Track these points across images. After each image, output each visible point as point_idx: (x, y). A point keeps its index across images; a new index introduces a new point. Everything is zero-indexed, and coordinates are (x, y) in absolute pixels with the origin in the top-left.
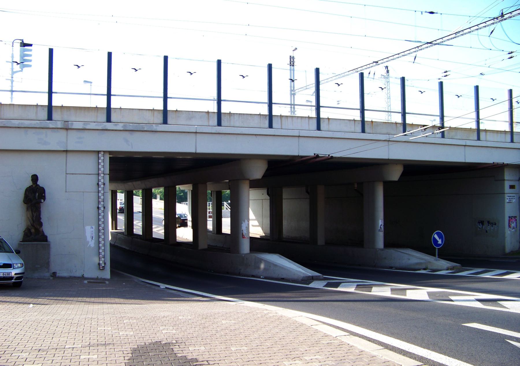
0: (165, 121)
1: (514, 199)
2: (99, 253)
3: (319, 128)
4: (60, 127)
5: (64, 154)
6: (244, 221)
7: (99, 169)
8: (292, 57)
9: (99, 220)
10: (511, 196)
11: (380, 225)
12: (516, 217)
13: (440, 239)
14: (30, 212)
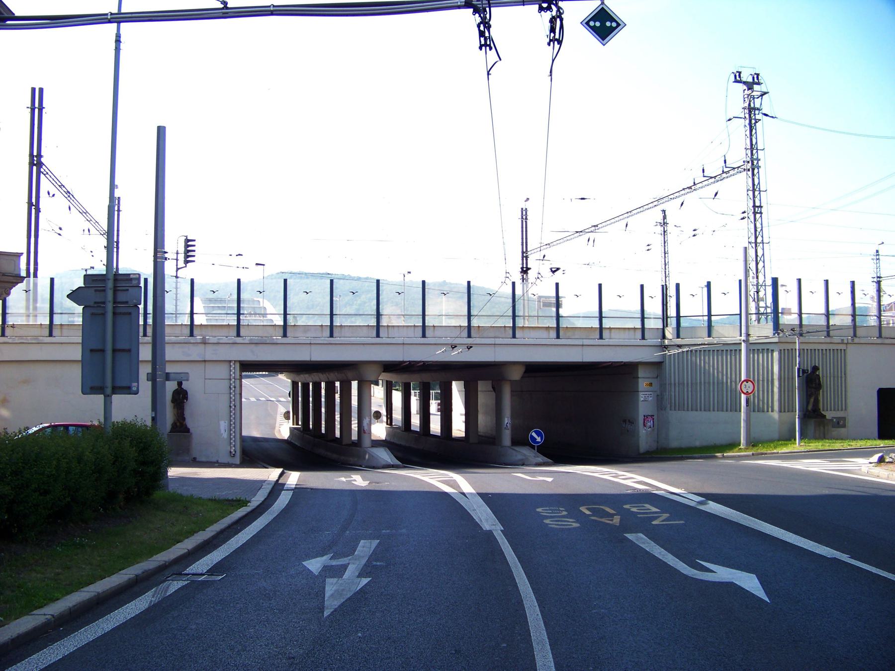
0: (285, 335)
1: (651, 397)
2: (231, 443)
3: (424, 336)
4: (199, 342)
5: (203, 363)
6: (365, 418)
7: (231, 375)
8: (524, 209)
9: (231, 416)
10: (646, 394)
11: (506, 422)
12: (654, 416)
13: (539, 437)
14: (176, 409)
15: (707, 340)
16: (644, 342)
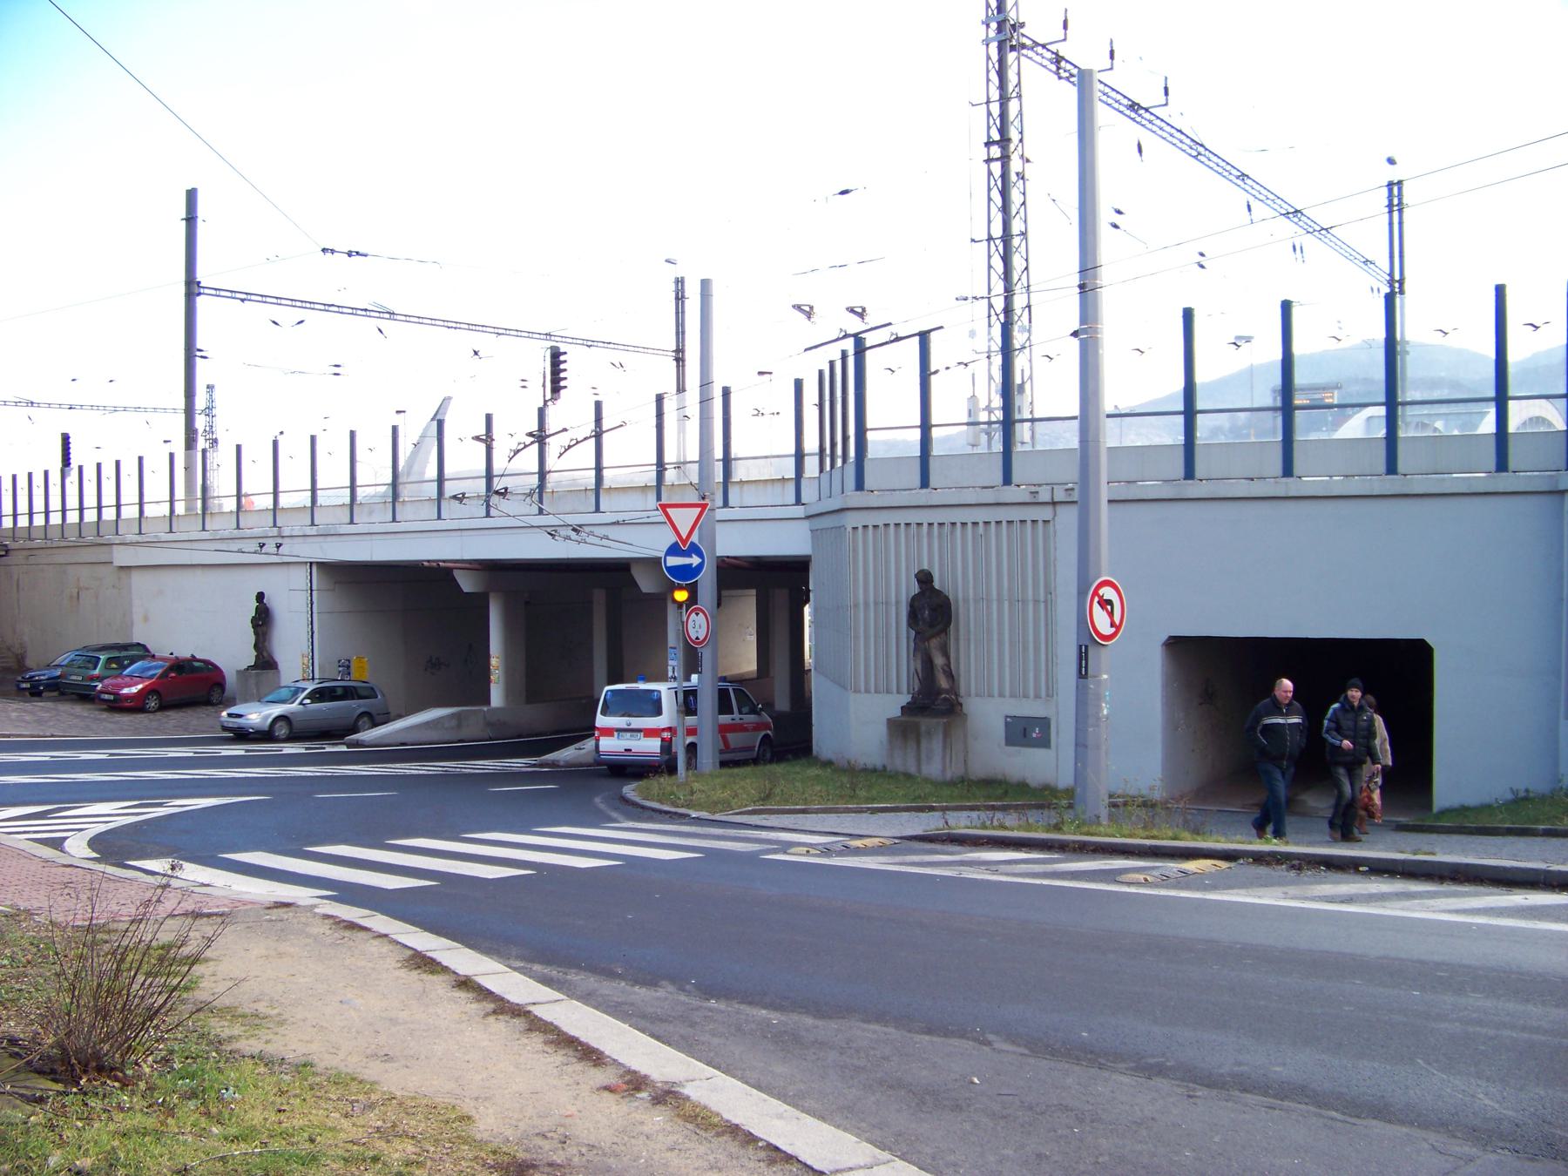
15: (1104, 496)
16: (1504, 482)
